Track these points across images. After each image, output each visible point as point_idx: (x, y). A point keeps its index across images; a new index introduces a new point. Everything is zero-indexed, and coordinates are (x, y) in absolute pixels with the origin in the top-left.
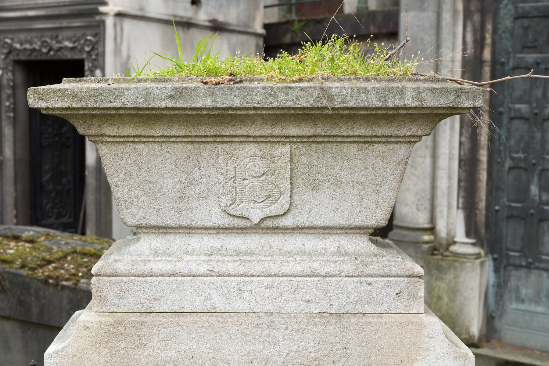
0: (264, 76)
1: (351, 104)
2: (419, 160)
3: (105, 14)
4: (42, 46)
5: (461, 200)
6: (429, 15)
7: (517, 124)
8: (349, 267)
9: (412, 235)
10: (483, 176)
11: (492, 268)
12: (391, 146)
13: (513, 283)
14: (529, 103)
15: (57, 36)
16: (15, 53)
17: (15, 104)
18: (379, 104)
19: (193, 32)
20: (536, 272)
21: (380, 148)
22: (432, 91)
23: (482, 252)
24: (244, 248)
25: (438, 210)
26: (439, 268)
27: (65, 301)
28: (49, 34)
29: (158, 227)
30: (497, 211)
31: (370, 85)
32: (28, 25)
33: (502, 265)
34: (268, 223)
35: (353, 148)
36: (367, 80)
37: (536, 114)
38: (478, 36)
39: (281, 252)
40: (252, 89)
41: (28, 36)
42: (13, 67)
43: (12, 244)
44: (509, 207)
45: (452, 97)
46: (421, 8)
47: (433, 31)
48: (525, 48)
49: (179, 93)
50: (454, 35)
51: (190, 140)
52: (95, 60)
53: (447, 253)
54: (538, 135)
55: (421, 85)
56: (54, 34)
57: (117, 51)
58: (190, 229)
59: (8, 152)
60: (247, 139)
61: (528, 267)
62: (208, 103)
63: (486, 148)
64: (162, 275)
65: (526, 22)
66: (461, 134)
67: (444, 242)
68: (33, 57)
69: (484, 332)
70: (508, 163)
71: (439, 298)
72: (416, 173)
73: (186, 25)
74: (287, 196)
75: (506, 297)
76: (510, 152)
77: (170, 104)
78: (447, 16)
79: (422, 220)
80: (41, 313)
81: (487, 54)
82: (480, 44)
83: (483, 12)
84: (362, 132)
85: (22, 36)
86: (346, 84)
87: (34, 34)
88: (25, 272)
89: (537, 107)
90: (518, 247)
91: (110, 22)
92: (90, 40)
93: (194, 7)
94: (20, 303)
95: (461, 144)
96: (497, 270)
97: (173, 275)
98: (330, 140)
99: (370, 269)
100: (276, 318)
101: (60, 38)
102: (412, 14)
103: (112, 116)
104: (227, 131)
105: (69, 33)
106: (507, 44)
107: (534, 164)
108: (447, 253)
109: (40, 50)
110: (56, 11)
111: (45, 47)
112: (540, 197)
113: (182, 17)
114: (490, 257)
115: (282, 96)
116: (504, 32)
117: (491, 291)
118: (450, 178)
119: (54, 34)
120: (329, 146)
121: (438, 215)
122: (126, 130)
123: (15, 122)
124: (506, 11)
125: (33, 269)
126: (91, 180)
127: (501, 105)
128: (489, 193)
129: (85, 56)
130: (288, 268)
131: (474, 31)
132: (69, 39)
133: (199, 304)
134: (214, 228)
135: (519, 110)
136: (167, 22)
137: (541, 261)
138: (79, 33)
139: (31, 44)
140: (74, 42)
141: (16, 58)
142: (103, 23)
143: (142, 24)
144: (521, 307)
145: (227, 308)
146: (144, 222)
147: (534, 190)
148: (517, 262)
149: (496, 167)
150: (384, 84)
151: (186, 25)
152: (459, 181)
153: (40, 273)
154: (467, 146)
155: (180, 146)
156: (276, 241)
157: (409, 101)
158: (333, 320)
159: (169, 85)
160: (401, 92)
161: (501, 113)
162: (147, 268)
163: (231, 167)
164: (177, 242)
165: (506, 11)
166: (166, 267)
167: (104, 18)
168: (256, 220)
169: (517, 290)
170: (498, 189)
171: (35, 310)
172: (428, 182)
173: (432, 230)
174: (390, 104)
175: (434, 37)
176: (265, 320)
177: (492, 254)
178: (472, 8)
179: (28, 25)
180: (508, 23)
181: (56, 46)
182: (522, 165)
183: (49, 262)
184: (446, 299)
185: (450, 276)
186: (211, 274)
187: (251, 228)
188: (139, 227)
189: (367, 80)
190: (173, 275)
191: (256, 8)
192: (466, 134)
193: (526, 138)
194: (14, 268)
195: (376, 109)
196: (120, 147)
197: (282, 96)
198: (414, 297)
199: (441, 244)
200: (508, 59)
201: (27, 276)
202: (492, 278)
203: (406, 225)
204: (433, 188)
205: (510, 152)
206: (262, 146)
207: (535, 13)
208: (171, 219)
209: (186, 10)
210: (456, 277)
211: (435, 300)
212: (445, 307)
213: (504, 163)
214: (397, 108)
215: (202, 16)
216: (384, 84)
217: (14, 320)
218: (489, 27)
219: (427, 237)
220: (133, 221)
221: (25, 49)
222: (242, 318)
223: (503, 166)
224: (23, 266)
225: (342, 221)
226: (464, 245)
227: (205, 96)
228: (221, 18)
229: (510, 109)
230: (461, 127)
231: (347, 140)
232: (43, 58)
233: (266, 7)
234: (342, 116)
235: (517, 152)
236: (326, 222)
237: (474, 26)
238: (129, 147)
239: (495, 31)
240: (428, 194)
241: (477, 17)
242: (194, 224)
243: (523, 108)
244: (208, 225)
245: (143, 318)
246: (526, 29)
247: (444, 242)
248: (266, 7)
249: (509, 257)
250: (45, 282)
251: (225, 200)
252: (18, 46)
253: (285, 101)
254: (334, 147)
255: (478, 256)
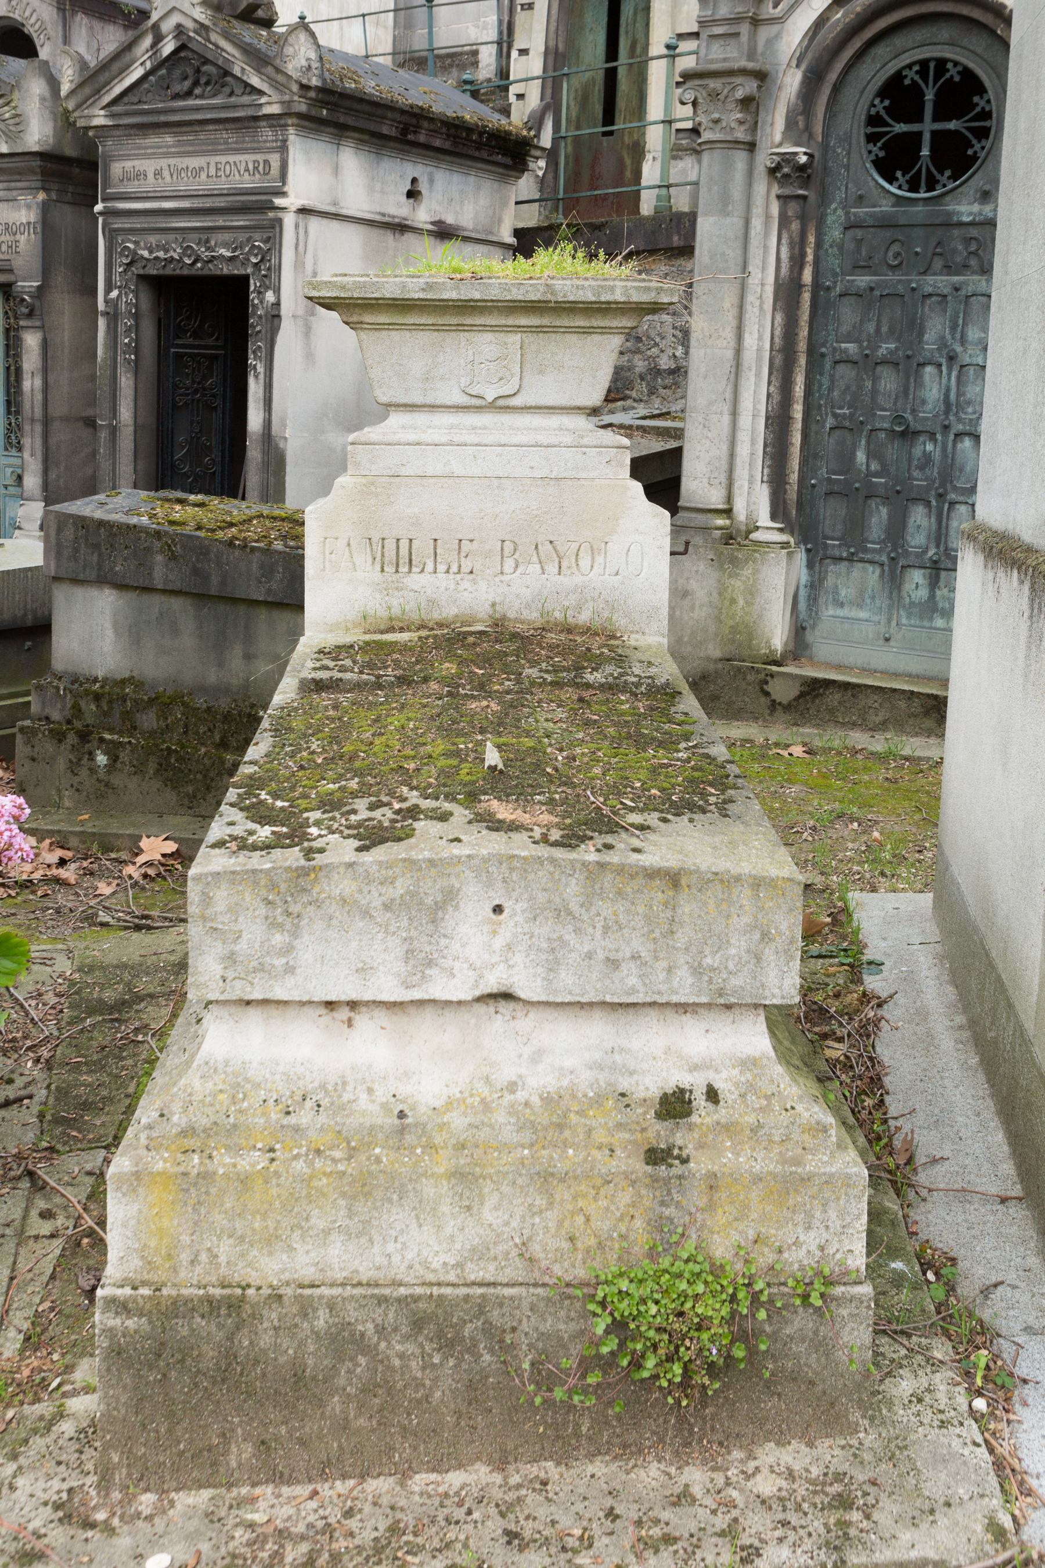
0: (501, 274)
1: (571, 298)
2: (714, 418)
3: (283, 209)
4: (184, 254)
5: (766, 471)
6: (735, 222)
7: (841, 369)
8: (568, 439)
9: (700, 519)
10: (797, 439)
11: (804, 562)
12: (606, 336)
13: (830, 581)
14: (858, 341)
15: (207, 241)
16: (140, 265)
17: (137, 341)
18: (594, 299)
19: (409, 237)
20: (860, 565)
21: (596, 338)
22: (637, 288)
23: (792, 540)
24: (479, 425)
25: (736, 485)
26: (733, 561)
27: (255, 566)
28: (195, 236)
29: (405, 405)
30: (813, 486)
31: (586, 283)
32: (162, 223)
33: (818, 558)
34: (501, 402)
35: (574, 338)
36: (586, 279)
37: (867, 356)
38: (797, 251)
39: (511, 428)
40: (490, 285)
41: (163, 239)
42: (137, 286)
43: (178, 507)
44: (829, 480)
45: (653, 294)
46: (724, 213)
47: (739, 243)
48: (858, 268)
49: (430, 287)
50: (766, 248)
51: (436, 328)
52: (265, 276)
53: (746, 542)
54: (869, 384)
55: (629, 284)
56: (204, 237)
57: (299, 265)
58: (433, 407)
59: (126, 413)
60: (485, 328)
61: (850, 559)
62: (454, 295)
63: (801, 401)
64: (409, 444)
65: (859, 233)
66: (769, 383)
67: (743, 528)
68: (168, 271)
69: (791, 647)
70: (830, 422)
71: (733, 601)
72: (710, 435)
73: (401, 228)
74: (517, 378)
75: (821, 601)
76: (833, 407)
77: (422, 296)
78: (757, 224)
79: (715, 499)
80: (223, 583)
81: (807, 276)
82: (798, 262)
83: (803, 218)
84: (582, 323)
85: (153, 239)
86: (568, 282)
87: (171, 237)
88: (202, 534)
89: (867, 348)
90: (838, 534)
91: (289, 220)
92: (259, 247)
93: (411, 201)
94: (196, 572)
95: (769, 395)
96: (810, 565)
97: (418, 444)
98: (554, 329)
99: (585, 441)
100: (503, 481)
101: (213, 243)
102: (711, 219)
103: (372, 305)
104: (468, 321)
105: (227, 236)
106: (833, 262)
107: (862, 423)
108: (746, 542)
109: (180, 261)
110: (208, 203)
111: (189, 256)
112: (868, 465)
113: (394, 217)
114: (803, 547)
115: (514, 291)
116: (831, 246)
117: (802, 592)
118: (753, 442)
119: (204, 237)
120: (554, 335)
121: (736, 491)
122: (383, 318)
123: (137, 368)
124: (834, 218)
125: (213, 531)
126: (254, 453)
127: (824, 345)
128: (804, 462)
129: (249, 270)
130: (515, 440)
131: (792, 245)
132: (226, 245)
133: (439, 470)
134: (453, 407)
135: (846, 351)
136: (370, 223)
137: (866, 550)
138: (242, 237)
139: (166, 251)
140: (234, 250)
141: (142, 272)
142: (280, 221)
143: (335, 225)
144: (840, 612)
145: (463, 473)
146: (394, 400)
147: (861, 456)
148: (836, 552)
149: (814, 427)
150: (599, 283)
151: (401, 228)
152: (765, 446)
153: (220, 534)
154: (776, 398)
155: (427, 333)
156: (507, 419)
157: (619, 296)
158: (552, 483)
159: (421, 280)
160: (612, 289)
161: (823, 355)
162: (395, 438)
163: (470, 352)
164: (421, 419)
165: (834, 218)
166: (412, 437)
167: (280, 215)
168: (490, 400)
169: (836, 592)
170: (816, 456)
171: (215, 580)
172: (725, 447)
173: (728, 512)
174: (603, 299)
175: (739, 252)
176: (496, 482)
177: (805, 544)
178: (790, 214)
179: (162, 223)
180: (837, 234)
181: (206, 255)
182: (847, 424)
183: (232, 525)
184: (741, 602)
185: (747, 572)
186: (451, 444)
187: (485, 407)
188: (389, 405)
189: (586, 279)
190: (418, 444)
191: (504, 204)
192: (776, 383)
193: (854, 388)
194: (188, 530)
195: (592, 303)
196: (376, 333)
197: (514, 291)
198: (621, 465)
199: (738, 531)
200: (835, 283)
201: (205, 538)
202: (804, 578)
203: (693, 505)
204: (732, 455)
205: (833, 407)
206: (497, 335)
207: (871, 222)
208: (418, 399)
209: (399, 205)
210: (756, 572)
211: (727, 603)
212: (740, 613)
213: (825, 421)
214: (609, 303)
215: (422, 216)
216: (599, 283)
217: (186, 594)
218: (811, 239)
219: (720, 522)
220: (384, 399)
221: (157, 258)
222: (476, 480)
223: (823, 427)
224: (199, 528)
225: (563, 401)
226: (768, 531)
227: (452, 289)
228: (450, 220)
229: (835, 349)
230: (770, 374)
231: (569, 330)
232: (185, 272)
233: (517, 203)
234: (564, 309)
235: (841, 408)
236: (550, 403)
237: (791, 237)
238: (384, 333)
239: (819, 245)
240: (724, 464)
241: (795, 226)
242: (438, 402)
243: (851, 347)
244: (449, 403)
245: (392, 480)
246: (859, 242)
247: (743, 528)
248: (517, 203)
249: (826, 546)
250: (230, 544)
251: (464, 382)
252: (145, 254)
253: (517, 295)
254: (558, 336)
255: (785, 545)
